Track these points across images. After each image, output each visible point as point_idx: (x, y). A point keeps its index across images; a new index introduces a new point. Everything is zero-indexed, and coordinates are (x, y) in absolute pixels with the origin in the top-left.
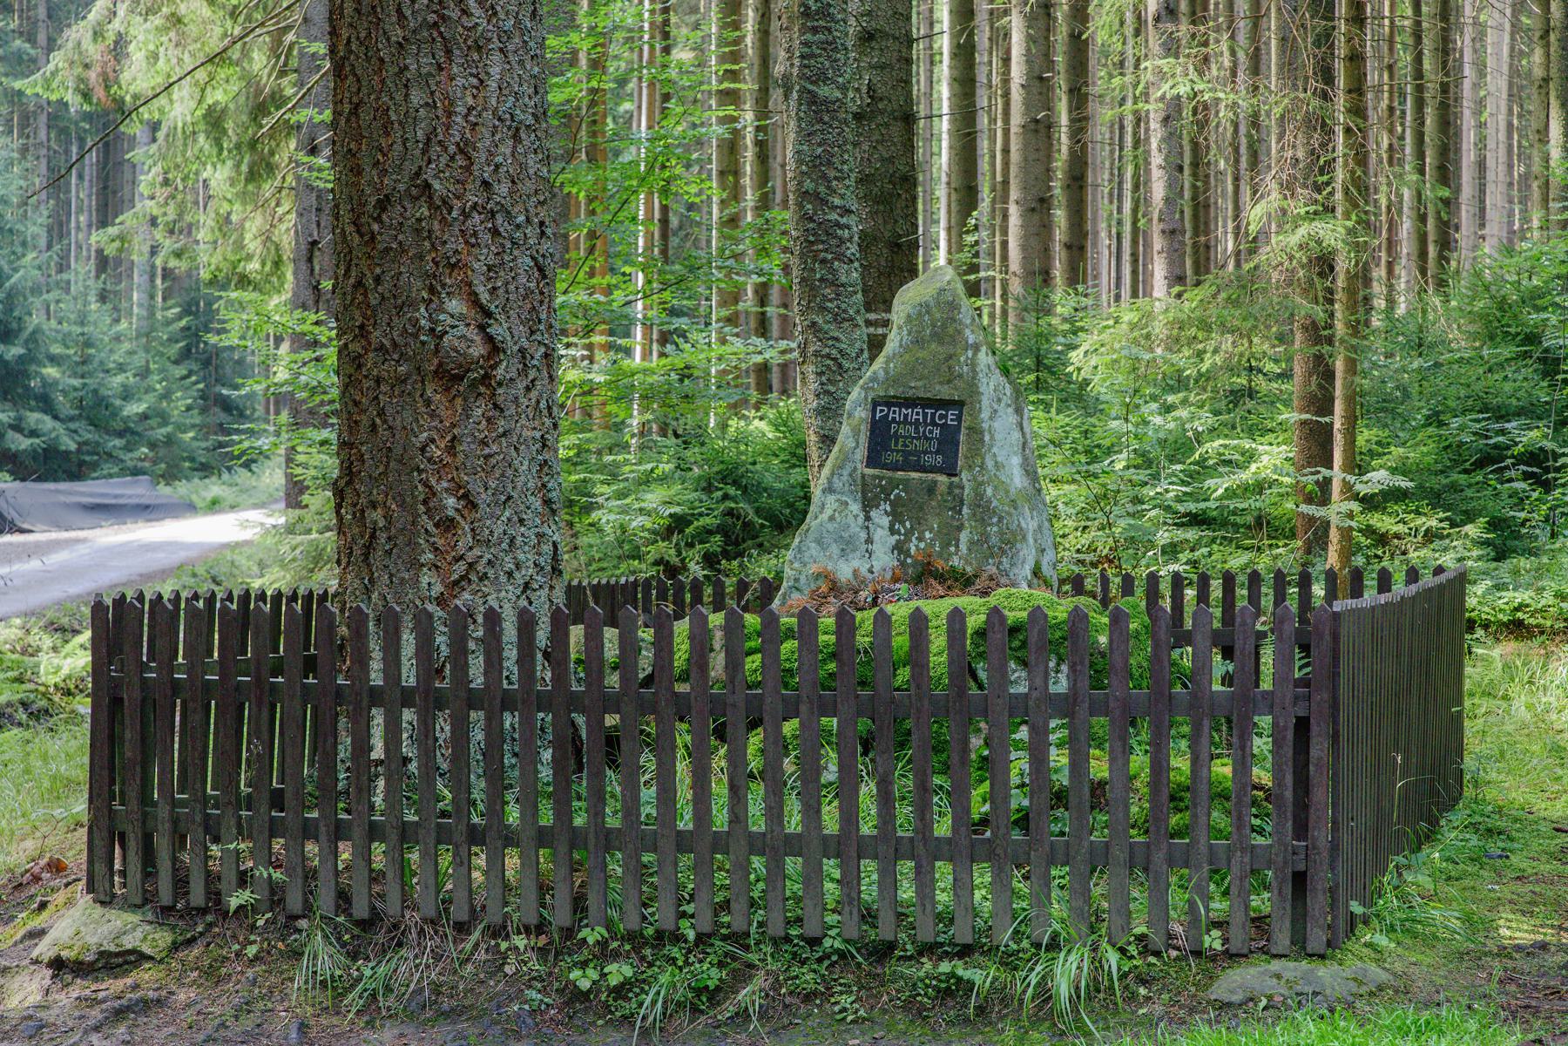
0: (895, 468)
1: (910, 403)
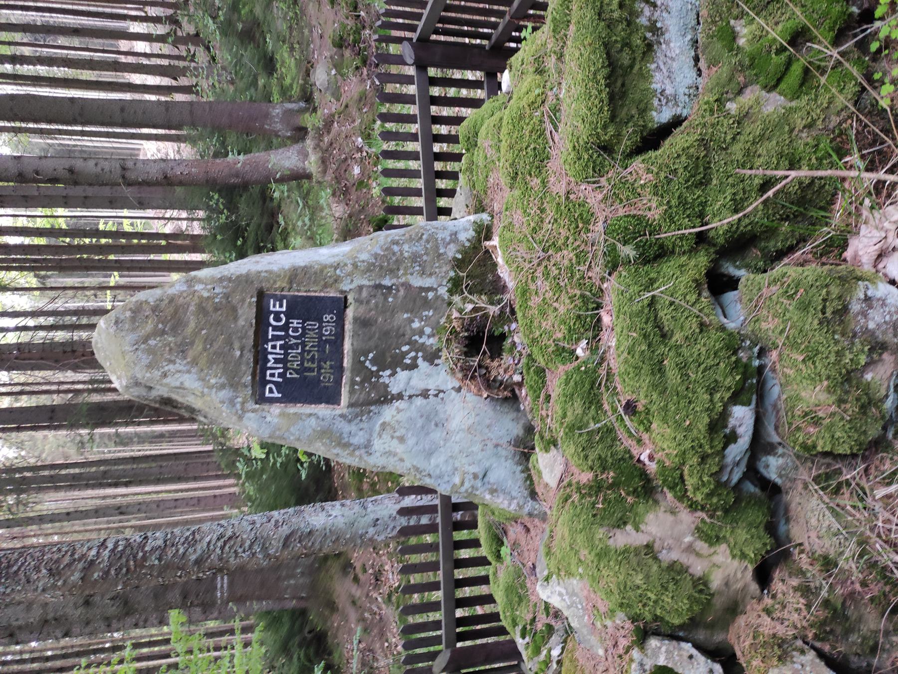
1: (260, 357)
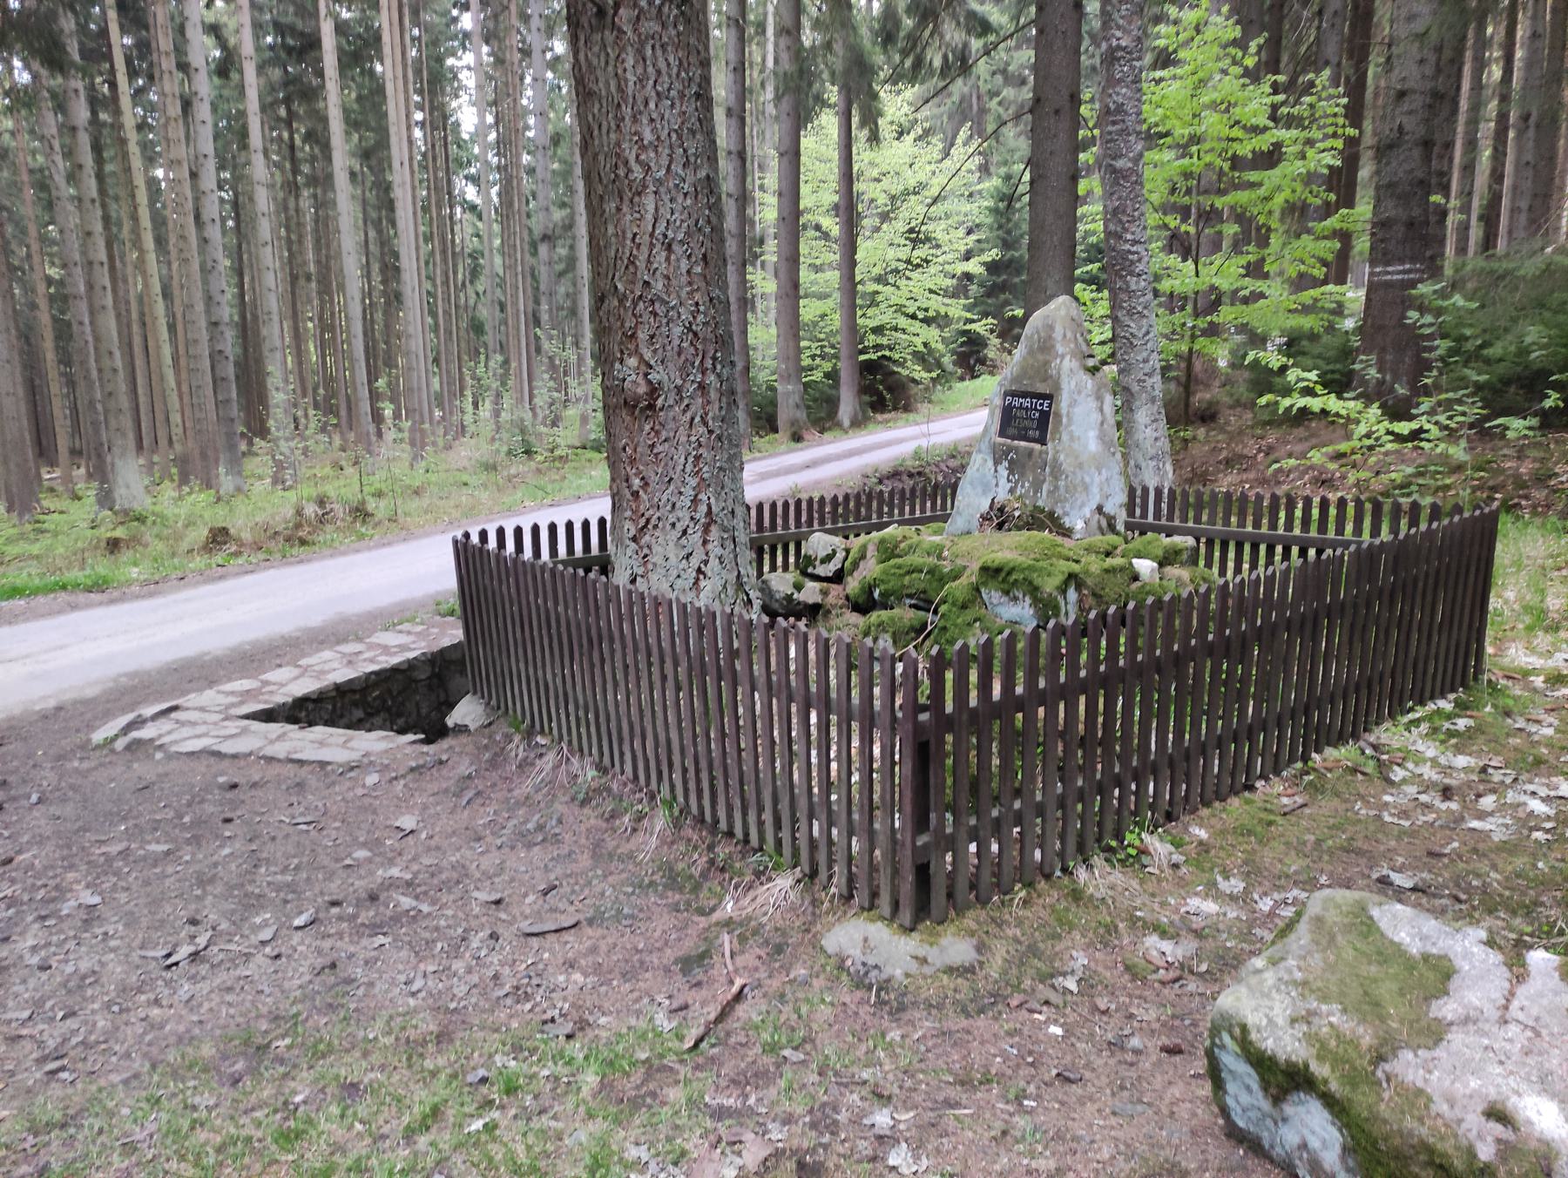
0: (1013, 439)
1: (1024, 395)
